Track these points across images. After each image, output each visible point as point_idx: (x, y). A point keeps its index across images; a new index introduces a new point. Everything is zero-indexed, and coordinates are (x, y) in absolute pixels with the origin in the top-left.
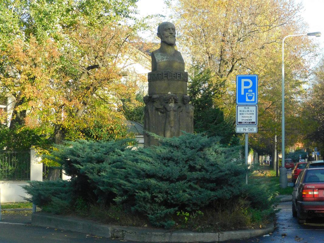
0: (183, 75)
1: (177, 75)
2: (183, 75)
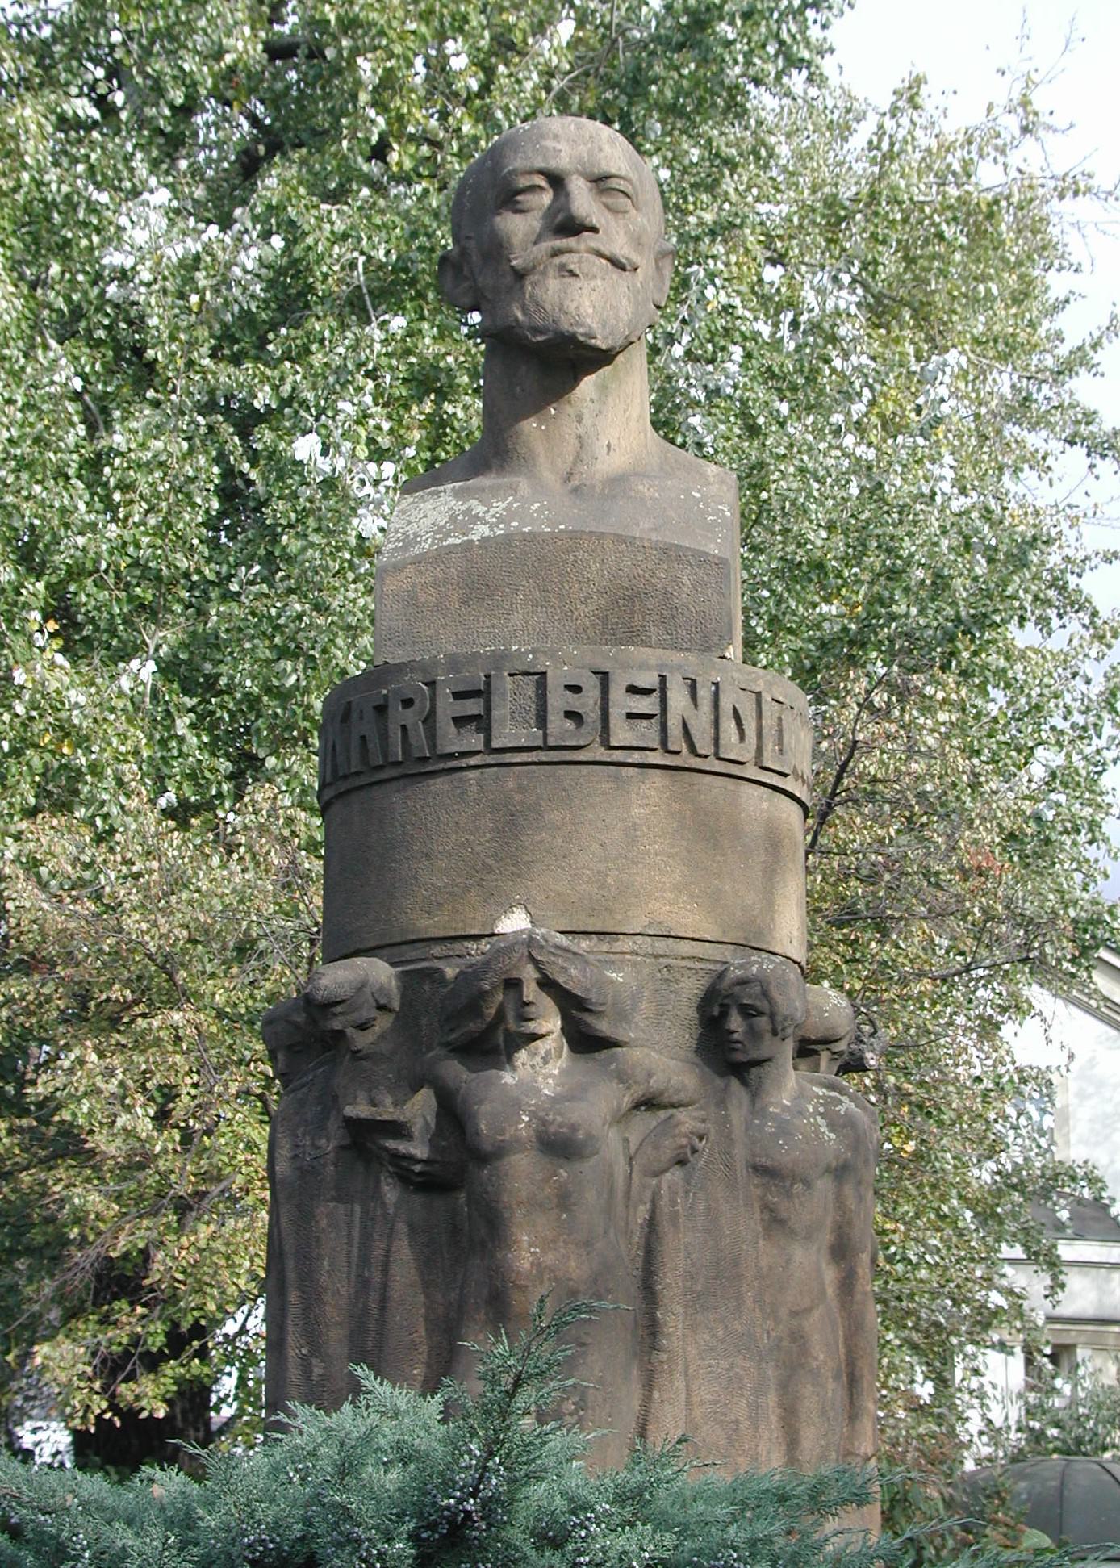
0: (705, 694)
1: (617, 693)
2: (705, 694)
